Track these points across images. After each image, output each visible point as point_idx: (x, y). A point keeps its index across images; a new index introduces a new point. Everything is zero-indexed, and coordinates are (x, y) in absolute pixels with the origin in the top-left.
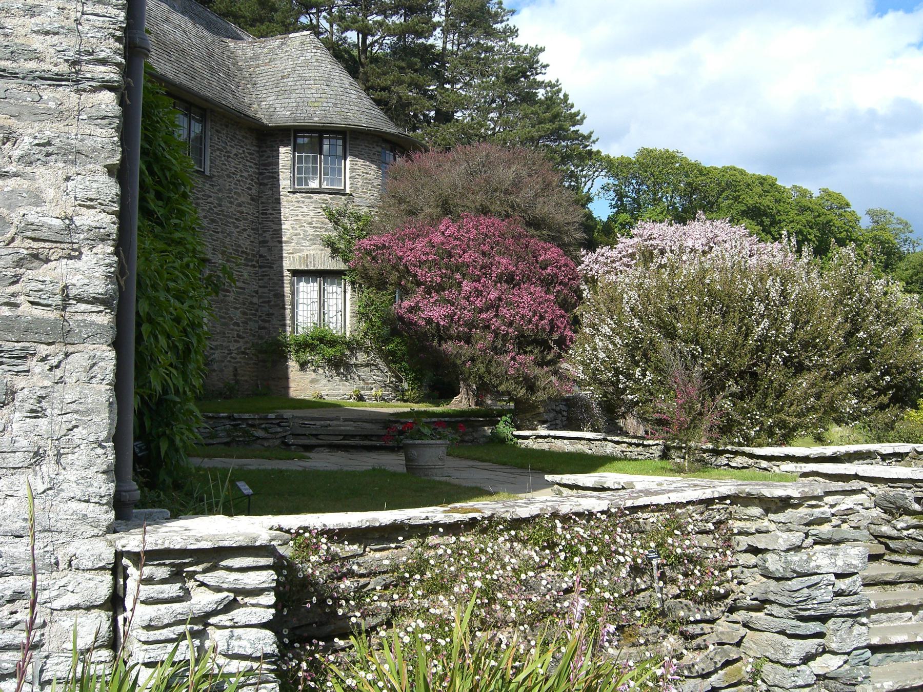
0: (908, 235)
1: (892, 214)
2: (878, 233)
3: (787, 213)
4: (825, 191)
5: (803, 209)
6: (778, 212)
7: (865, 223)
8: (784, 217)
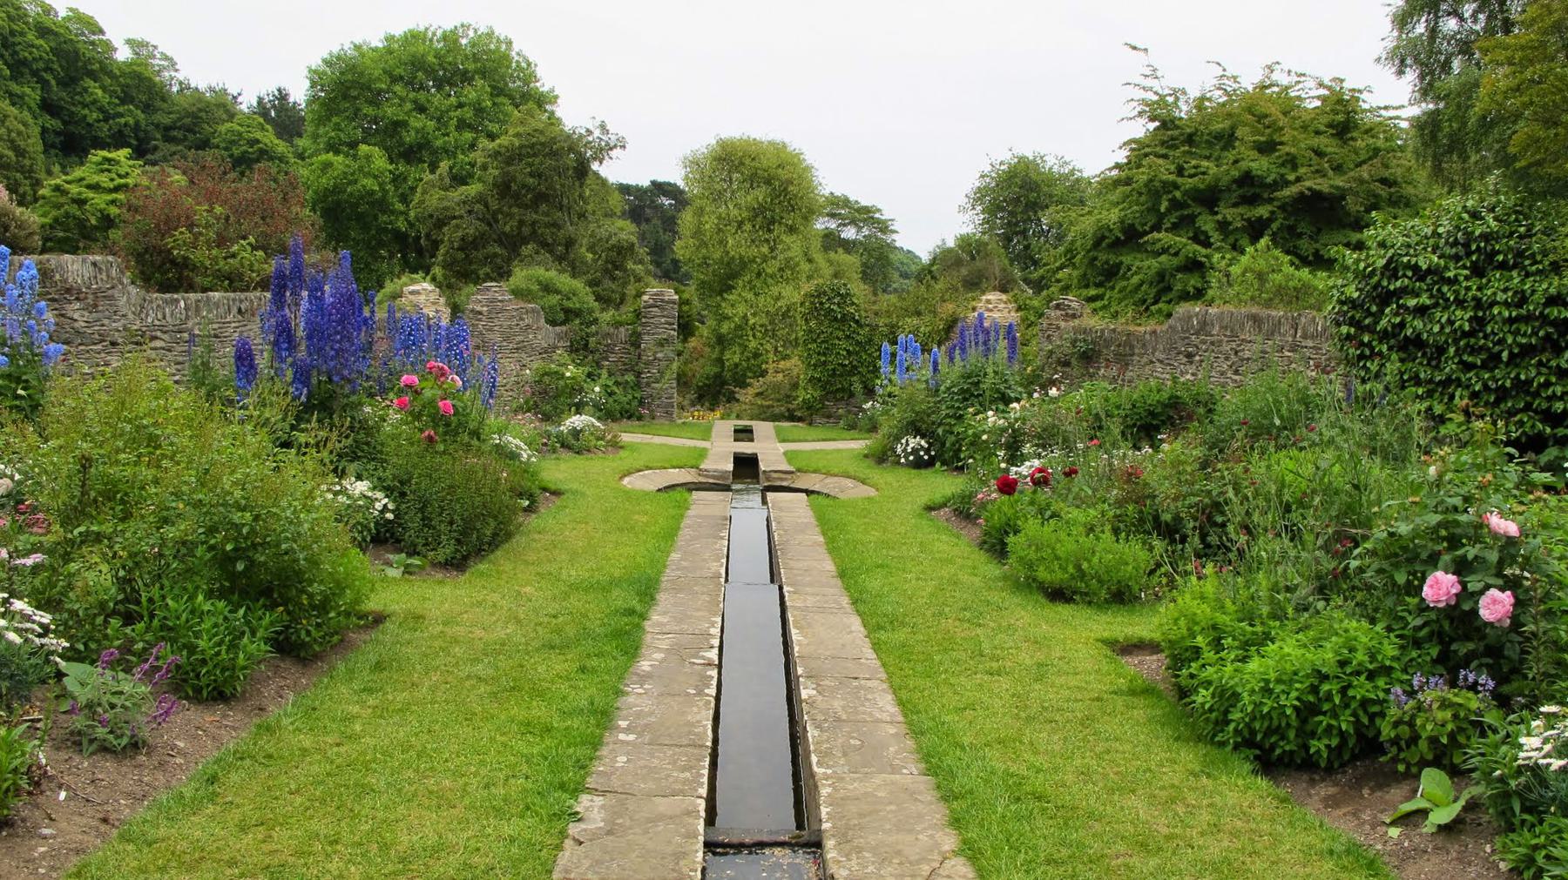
3: (22, 34)
4: (71, 10)
5: (44, 31)
6: (12, 33)
7: (123, 54)
8: (18, 39)
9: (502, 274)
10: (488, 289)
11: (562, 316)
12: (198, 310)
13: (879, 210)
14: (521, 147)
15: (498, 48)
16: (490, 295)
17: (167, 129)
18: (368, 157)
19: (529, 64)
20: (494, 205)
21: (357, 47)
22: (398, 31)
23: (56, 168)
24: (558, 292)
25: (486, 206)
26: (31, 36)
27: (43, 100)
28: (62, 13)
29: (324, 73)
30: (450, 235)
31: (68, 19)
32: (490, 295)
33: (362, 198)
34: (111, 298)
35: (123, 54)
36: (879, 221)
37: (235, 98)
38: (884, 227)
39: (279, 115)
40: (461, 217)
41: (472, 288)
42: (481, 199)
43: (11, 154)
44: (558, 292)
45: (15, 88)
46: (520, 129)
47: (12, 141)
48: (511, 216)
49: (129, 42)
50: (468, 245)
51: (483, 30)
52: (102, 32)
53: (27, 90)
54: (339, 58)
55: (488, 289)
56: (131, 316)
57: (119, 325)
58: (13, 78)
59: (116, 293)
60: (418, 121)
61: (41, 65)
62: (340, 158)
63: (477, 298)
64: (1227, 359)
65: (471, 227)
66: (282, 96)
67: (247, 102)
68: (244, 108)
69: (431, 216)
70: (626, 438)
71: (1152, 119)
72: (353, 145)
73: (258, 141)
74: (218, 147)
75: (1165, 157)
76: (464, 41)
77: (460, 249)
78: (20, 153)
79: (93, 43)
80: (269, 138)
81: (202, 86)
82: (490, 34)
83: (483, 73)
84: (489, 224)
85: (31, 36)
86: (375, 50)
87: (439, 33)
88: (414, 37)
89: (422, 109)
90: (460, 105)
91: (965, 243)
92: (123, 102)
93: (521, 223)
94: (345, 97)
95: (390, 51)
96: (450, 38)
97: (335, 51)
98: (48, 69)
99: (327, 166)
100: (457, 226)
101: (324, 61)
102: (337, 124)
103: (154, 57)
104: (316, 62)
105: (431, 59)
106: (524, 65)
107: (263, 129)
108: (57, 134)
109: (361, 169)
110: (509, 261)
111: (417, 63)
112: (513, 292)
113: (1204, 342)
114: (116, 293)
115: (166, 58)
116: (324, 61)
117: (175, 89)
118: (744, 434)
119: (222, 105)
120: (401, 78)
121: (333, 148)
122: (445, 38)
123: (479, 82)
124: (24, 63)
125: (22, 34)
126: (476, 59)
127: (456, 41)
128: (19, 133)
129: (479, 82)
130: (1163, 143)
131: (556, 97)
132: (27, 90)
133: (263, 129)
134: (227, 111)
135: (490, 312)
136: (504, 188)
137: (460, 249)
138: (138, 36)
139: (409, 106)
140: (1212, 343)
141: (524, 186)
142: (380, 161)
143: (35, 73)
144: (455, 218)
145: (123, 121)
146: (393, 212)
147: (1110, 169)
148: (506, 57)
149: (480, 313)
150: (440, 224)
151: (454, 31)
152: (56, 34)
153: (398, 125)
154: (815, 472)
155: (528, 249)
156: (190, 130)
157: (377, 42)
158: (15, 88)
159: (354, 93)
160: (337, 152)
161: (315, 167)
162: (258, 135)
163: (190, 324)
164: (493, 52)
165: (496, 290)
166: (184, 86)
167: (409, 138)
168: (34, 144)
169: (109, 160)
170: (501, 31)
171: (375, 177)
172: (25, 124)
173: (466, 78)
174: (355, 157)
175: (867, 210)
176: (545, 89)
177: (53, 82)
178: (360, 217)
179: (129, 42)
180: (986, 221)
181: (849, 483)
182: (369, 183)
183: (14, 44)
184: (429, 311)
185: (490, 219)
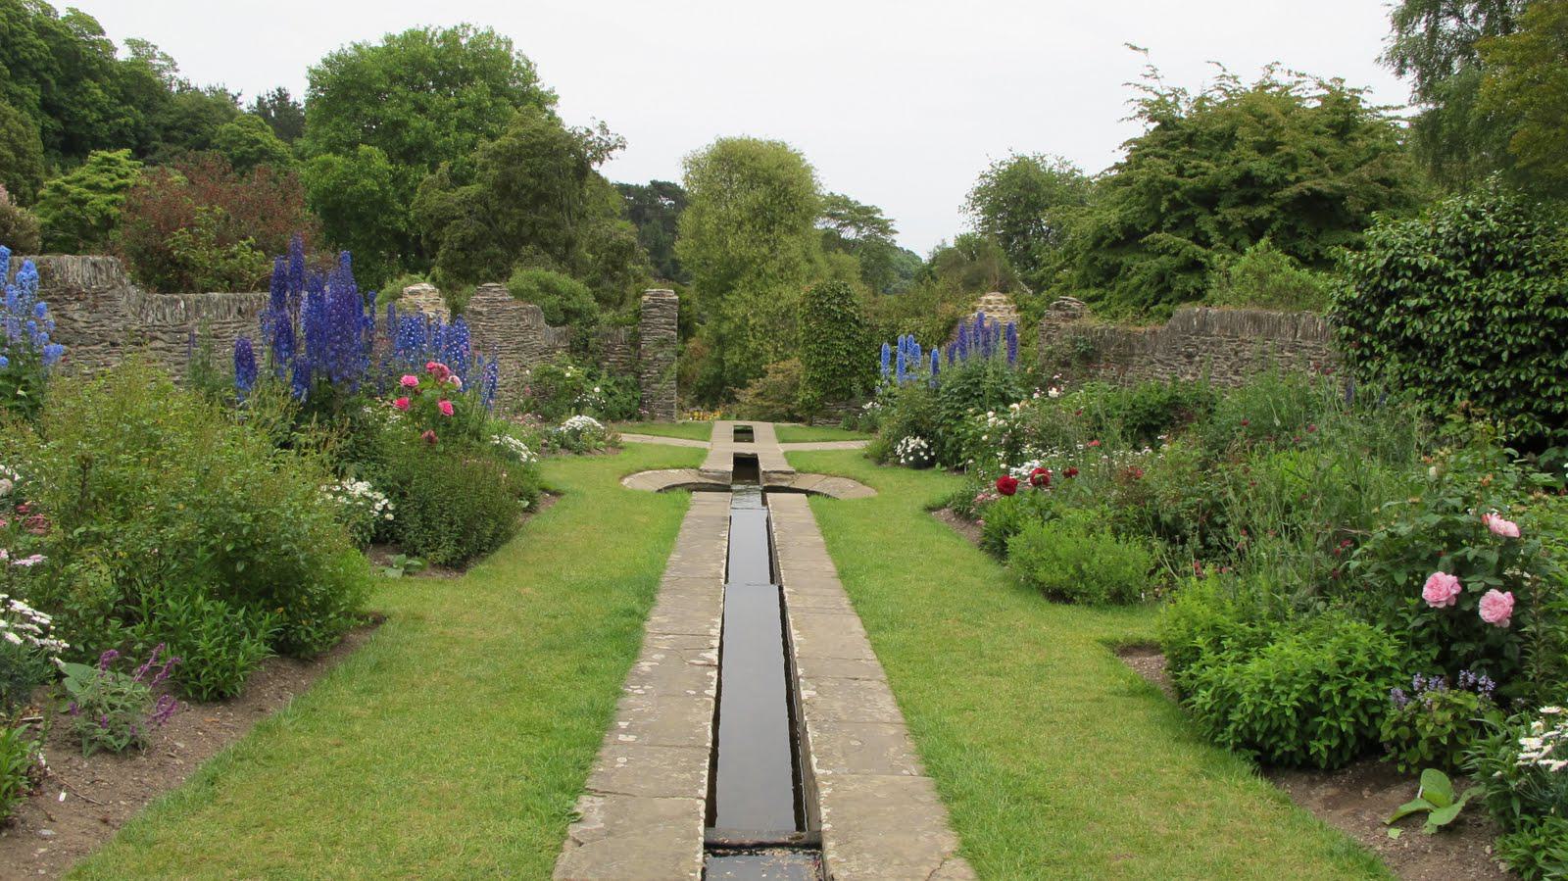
0: (173, 74)
1: (155, 47)
2: (137, 69)
3: (23, 34)
5: (43, 31)
7: (123, 54)
8: (19, 39)
9: (503, 275)
10: (488, 289)
11: (561, 317)
12: (198, 311)
13: (879, 211)
14: (522, 147)
15: (498, 48)
16: (490, 295)
17: (167, 129)
18: (368, 157)
19: (529, 64)
20: (494, 205)
21: (357, 48)
22: (398, 32)
23: (56, 169)
24: (558, 293)
25: (486, 205)
26: (31, 36)
27: (43, 100)
28: (62, 13)
29: (324, 73)
30: (450, 235)
31: (68, 19)
32: (490, 295)
33: (362, 197)
34: (111, 298)
35: (123, 54)
36: (878, 222)
37: (234, 98)
38: (884, 227)
39: (278, 113)
40: (461, 217)
41: (471, 288)
42: (481, 199)
43: (10, 154)
44: (558, 293)
45: (14, 87)
46: (520, 129)
47: (11, 141)
48: (510, 216)
49: (129, 42)
50: (467, 246)
51: (482, 30)
52: (102, 32)
53: (28, 91)
54: (339, 58)
55: (488, 289)
56: (131, 316)
57: (119, 325)
58: (14, 78)
59: (116, 293)
60: (417, 122)
61: (41, 65)
62: (340, 159)
63: (480, 298)
64: (1227, 359)
65: (471, 228)
66: (282, 96)
67: (247, 102)
68: (244, 108)
69: (431, 216)
70: (626, 438)
71: (1152, 119)
72: (353, 145)
73: (258, 142)
74: (218, 147)
75: (1164, 157)
76: (464, 42)
77: (462, 249)
78: (20, 153)
79: (93, 43)
80: (269, 138)
81: (202, 87)
82: (490, 35)
83: (483, 73)
84: (489, 224)
85: (31, 36)
86: (375, 50)
87: (439, 33)
88: (414, 37)
89: (422, 109)
90: (460, 106)
91: (965, 242)
92: (123, 102)
93: (521, 223)
94: (346, 97)
95: (389, 51)
96: (451, 38)
97: (335, 51)
98: (48, 69)
99: (327, 165)
100: (458, 226)
101: (325, 61)
102: (338, 125)
103: (154, 57)
104: (316, 63)
105: (431, 59)
106: (524, 65)
107: (263, 129)
108: (58, 134)
109: (361, 168)
110: (509, 261)
111: (417, 64)
112: (513, 292)
113: (1204, 342)
114: (116, 293)
115: (166, 58)
116: (325, 61)
117: (175, 89)
118: (744, 434)
119: (220, 105)
120: (401, 78)
121: (333, 148)
122: (445, 38)
123: (479, 82)
124: (24, 63)
125: (23, 34)
126: (476, 58)
127: (456, 41)
128: (19, 133)
129: (479, 82)
130: (1163, 143)
131: (556, 97)
132: (28, 91)
133: (263, 129)
134: (227, 111)
135: (489, 312)
136: (504, 188)
137: (462, 249)
138: (137, 37)
139: (408, 106)
140: (1212, 344)
141: (524, 186)
142: (380, 161)
143: (35, 74)
144: (455, 218)
145: (122, 121)
146: (392, 212)
147: (1110, 169)
148: (507, 58)
149: (480, 313)
150: (440, 224)
151: (454, 32)
152: (56, 34)
153: (398, 126)
154: (815, 472)
155: (527, 250)
156: (190, 131)
157: (377, 41)
158: (14, 87)
159: (354, 93)
160: (337, 153)
161: (316, 168)
162: (258, 135)
163: (190, 324)
164: (493, 52)
165: (496, 290)
166: (184, 87)
167: (409, 138)
168: (34, 144)
169: (109, 160)
170: (501, 32)
171: (375, 177)
172: (25, 125)
173: (466, 77)
174: (355, 157)
175: (867, 210)
176: (544, 89)
177: (53, 82)
178: (360, 218)
179: (129, 42)
180: (985, 222)
181: (850, 483)
182: (369, 183)
183: (14, 44)
184: (429, 312)
185: (490, 219)
